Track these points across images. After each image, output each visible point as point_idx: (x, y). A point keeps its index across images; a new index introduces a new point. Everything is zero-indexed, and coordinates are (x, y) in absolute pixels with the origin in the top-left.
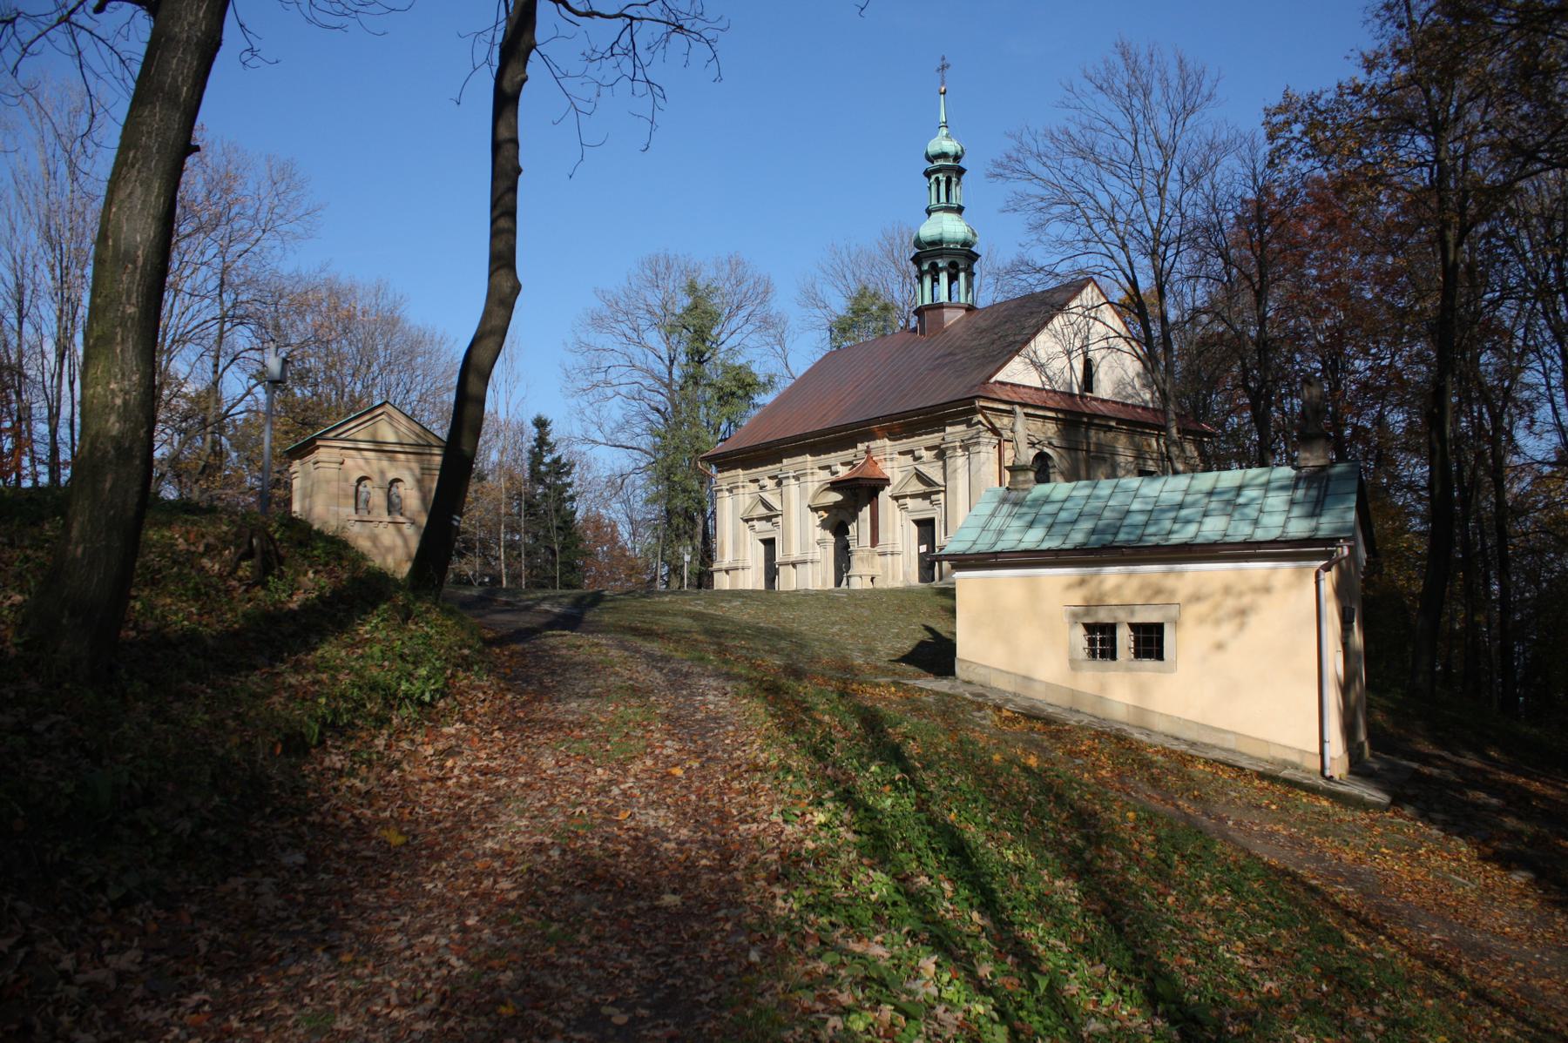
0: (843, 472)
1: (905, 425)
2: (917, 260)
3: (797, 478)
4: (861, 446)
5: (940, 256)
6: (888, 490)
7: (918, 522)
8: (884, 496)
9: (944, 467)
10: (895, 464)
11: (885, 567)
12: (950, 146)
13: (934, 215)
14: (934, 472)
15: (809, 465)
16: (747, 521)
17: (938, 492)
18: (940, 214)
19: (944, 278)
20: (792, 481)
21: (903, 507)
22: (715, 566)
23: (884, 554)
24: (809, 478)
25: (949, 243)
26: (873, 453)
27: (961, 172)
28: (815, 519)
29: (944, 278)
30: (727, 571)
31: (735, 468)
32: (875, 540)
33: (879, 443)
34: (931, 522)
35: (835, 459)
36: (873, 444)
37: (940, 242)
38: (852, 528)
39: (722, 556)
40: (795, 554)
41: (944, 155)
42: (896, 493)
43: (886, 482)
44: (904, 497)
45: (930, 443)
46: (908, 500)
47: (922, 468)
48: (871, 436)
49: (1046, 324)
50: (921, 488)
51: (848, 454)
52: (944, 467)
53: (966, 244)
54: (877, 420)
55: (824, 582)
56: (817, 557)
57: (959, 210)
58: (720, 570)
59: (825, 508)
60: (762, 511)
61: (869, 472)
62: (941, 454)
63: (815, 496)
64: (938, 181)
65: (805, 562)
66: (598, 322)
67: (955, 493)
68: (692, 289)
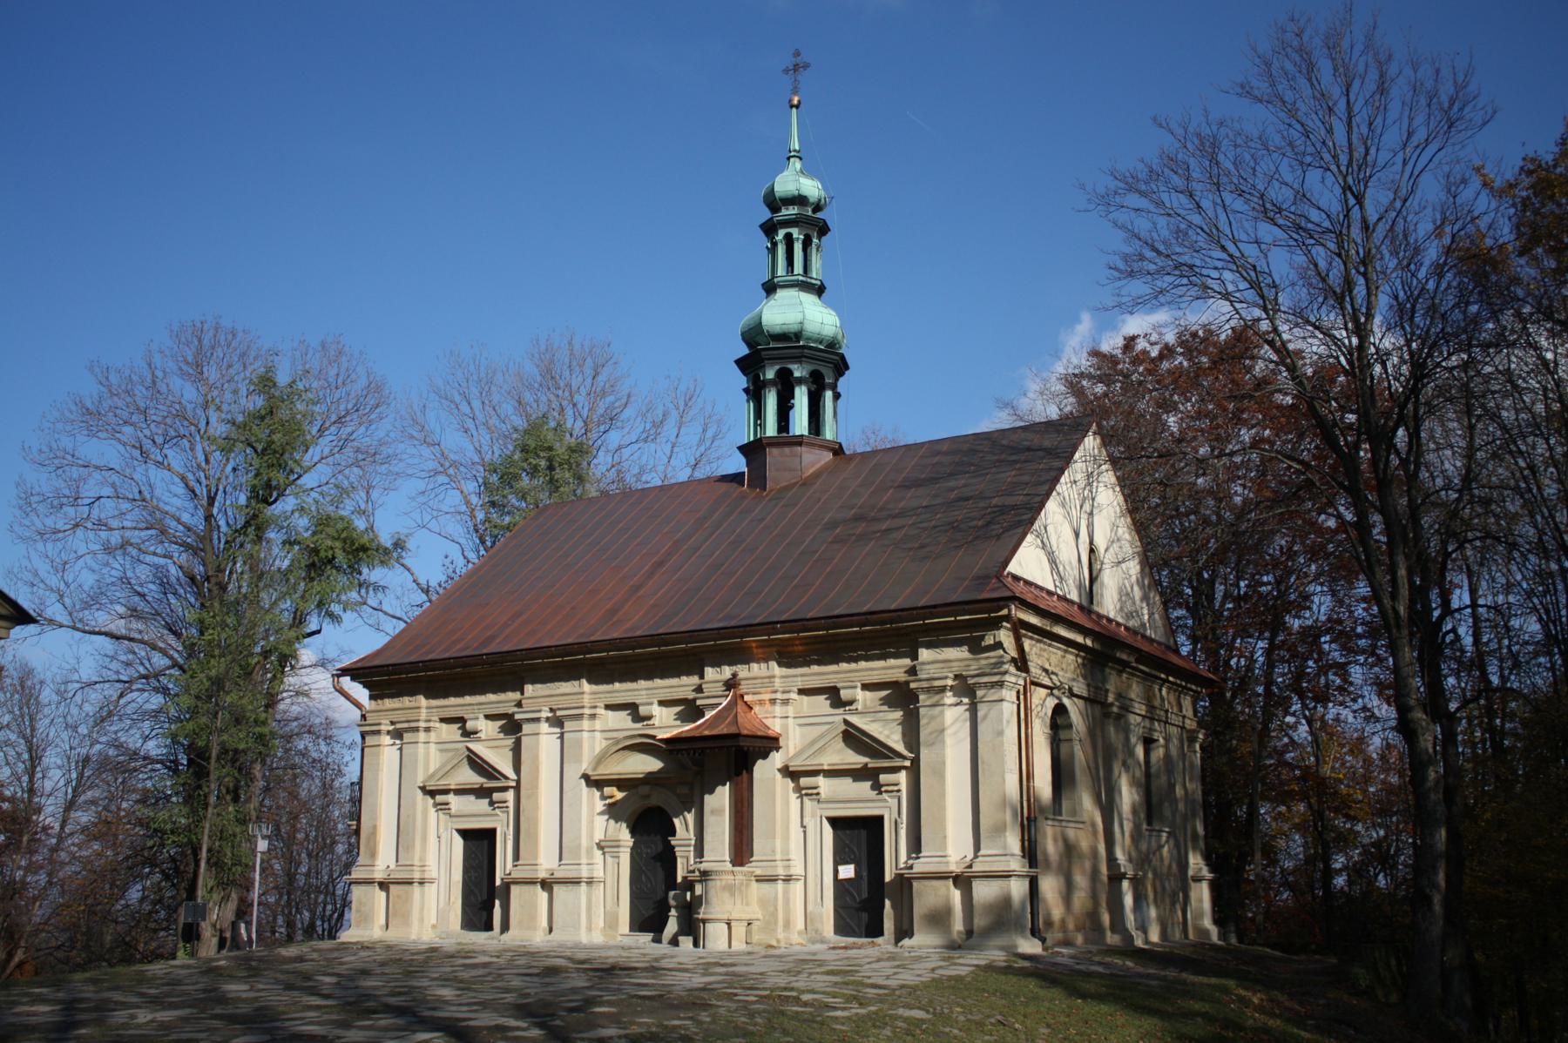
0: (666, 723)
1: (815, 641)
2: (747, 365)
3: (397, 735)
4: (715, 675)
5: (798, 359)
6: (777, 759)
7: (464, 833)
8: (766, 771)
9: (517, 750)
10: (790, 710)
11: (768, 904)
12: (811, 188)
13: (781, 294)
14: (887, 729)
15: (424, 714)
16: (432, 793)
17: (505, 789)
18: (792, 293)
19: (801, 398)
20: (387, 740)
21: (443, 807)
22: (356, 874)
23: (772, 879)
24: (422, 736)
25: (809, 339)
26: (743, 688)
27: (823, 229)
28: (591, 804)
29: (801, 398)
30: (384, 885)
31: (412, 693)
32: (742, 850)
33: (757, 669)
34: (491, 833)
35: (643, 691)
36: (743, 671)
37: (798, 335)
38: (684, 827)
39: (373, 854)
40: (546, 861)
41: (800, 200)
42: (796, 765)
43: (769, 744)
44: (446, 792)
45: (875, 677)
46: (451, 798)
47: (477, 748)
48: (740, 655)
49: (1052, 489)
50: (474, 779)
51: (683, 686)
52: (517, 750)
53: (833, 345)
54: (768, 626)
55: (611, 923)
56: (598, 873)
57: (819, 290)
58: (369, 882)
59: (620, 783)
60: (470, 777)
61: (747, 724)
62: (902, 697)
63: (600, 760)
64: (789, 239)
65: (575, 882)
66: (92, 418)
67: (940, 773)
68: (266, 383)
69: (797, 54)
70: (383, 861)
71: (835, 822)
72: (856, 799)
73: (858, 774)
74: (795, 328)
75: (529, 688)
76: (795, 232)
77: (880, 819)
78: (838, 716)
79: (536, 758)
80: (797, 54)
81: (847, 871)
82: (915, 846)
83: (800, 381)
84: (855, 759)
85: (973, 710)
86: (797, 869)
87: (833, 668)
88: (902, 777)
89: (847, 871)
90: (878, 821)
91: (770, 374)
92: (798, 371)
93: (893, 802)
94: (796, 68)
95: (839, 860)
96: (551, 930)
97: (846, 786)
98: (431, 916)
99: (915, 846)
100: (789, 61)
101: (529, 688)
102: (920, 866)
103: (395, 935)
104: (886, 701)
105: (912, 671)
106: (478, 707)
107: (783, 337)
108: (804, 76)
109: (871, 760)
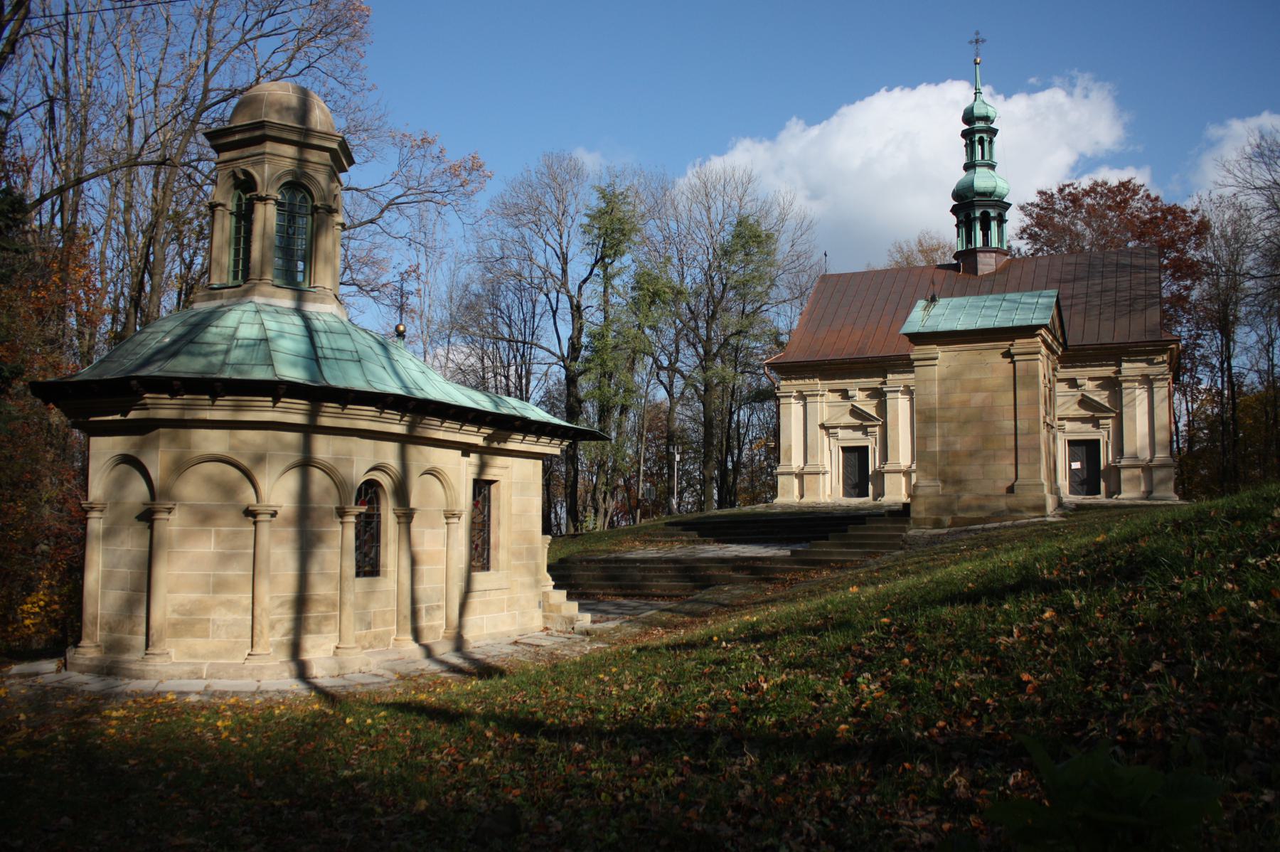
14: (870, 408)
22: (779, 470)
39: (790, 459)
62: (879, 395)
67: (1133, 419)
69: (977, 33)
70: (797, 462)
71: (843, 448)
72: (856, 439)
73: (1083, 420)
74: (991, 190)
75: (890, 376)
76: (985, 136)
77: (1098, 441)
78: (848, 404)
79: (896, 411)
80: (977, 33)
81: (1076, 465)
82: (884, 458)
83: (994, 218)
84: (857, 422)
85: (805, 407)
86: (828, 469)
87: (801, 382)
88: (877, 429)
89: (1076, 465)
90: (866, 448)
91: (978, 214)
92: (993, 213)
93: (1105, 433)
94: (977, 41)
95: (1072, 459)
96: (802, 496)
97: (1077, 425)
98: (829, 490)
99: (884, 458)
100: (974, 37)
101: (890, 376)
102: (887, 467)
103: (809, 499)
104: (868, 396)
105: (1119, 372)
106: (858, 389)
107: (983, 194)
108: (982, 46)
109: (861, 420)
